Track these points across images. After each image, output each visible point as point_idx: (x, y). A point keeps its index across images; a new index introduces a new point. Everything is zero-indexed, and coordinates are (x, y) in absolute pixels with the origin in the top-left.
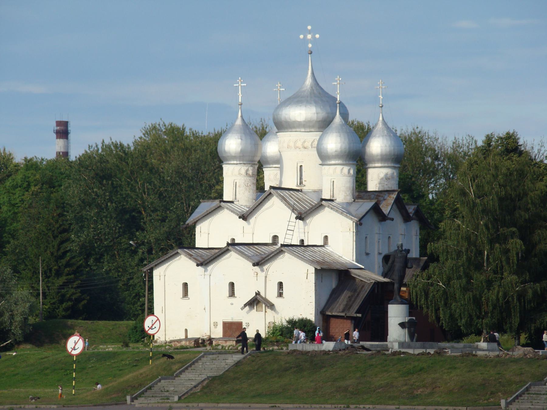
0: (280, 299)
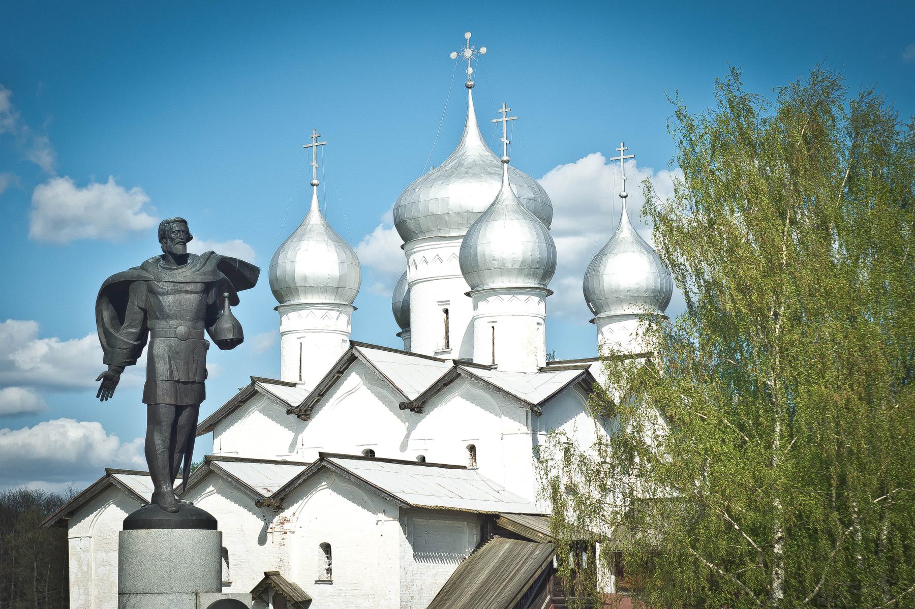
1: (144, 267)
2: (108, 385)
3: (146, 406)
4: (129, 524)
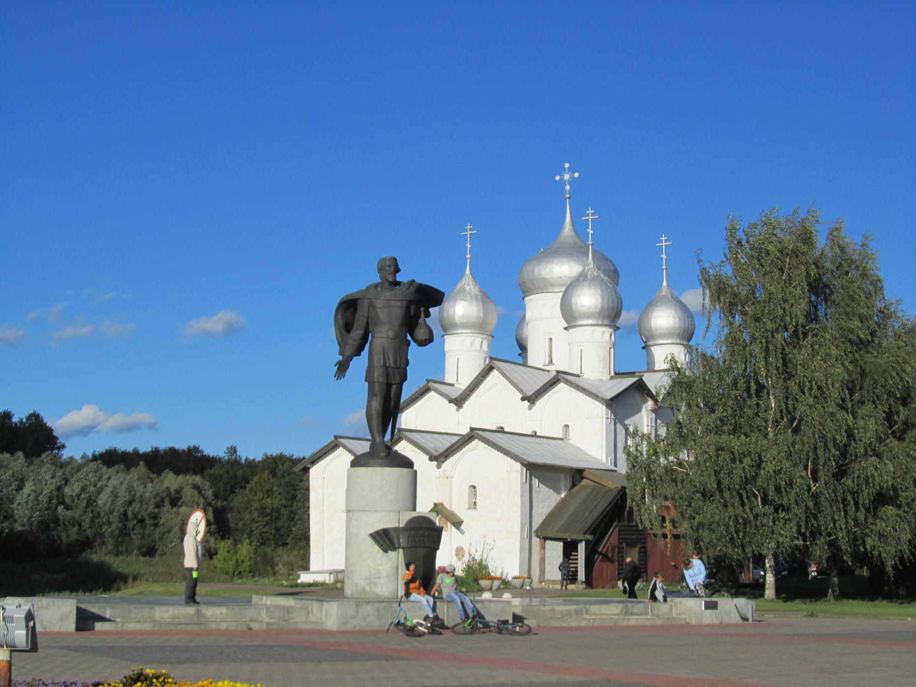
0: (473, 512)
1: (368, 289)
2: (342, 368)
3: (367, 384)
4: (354, 464)
